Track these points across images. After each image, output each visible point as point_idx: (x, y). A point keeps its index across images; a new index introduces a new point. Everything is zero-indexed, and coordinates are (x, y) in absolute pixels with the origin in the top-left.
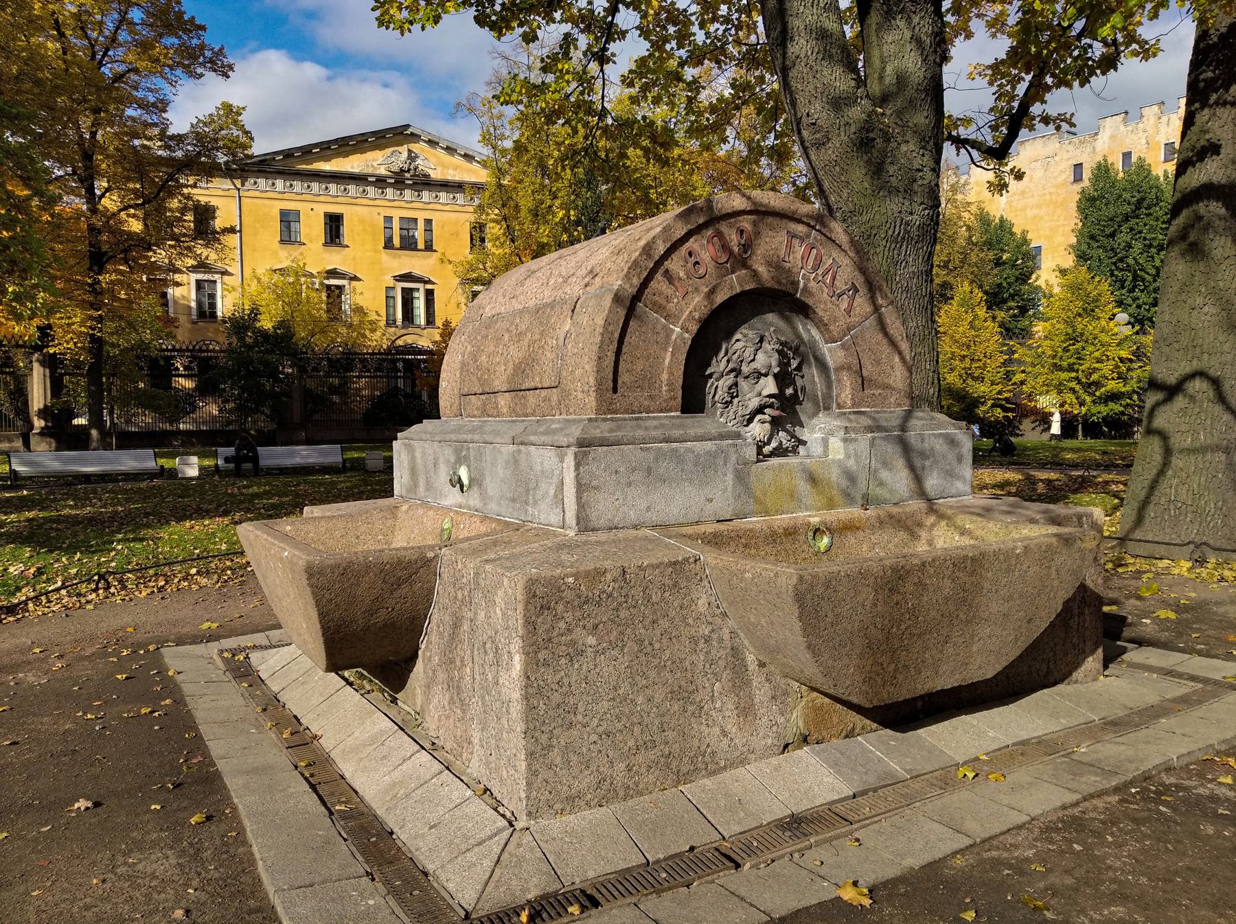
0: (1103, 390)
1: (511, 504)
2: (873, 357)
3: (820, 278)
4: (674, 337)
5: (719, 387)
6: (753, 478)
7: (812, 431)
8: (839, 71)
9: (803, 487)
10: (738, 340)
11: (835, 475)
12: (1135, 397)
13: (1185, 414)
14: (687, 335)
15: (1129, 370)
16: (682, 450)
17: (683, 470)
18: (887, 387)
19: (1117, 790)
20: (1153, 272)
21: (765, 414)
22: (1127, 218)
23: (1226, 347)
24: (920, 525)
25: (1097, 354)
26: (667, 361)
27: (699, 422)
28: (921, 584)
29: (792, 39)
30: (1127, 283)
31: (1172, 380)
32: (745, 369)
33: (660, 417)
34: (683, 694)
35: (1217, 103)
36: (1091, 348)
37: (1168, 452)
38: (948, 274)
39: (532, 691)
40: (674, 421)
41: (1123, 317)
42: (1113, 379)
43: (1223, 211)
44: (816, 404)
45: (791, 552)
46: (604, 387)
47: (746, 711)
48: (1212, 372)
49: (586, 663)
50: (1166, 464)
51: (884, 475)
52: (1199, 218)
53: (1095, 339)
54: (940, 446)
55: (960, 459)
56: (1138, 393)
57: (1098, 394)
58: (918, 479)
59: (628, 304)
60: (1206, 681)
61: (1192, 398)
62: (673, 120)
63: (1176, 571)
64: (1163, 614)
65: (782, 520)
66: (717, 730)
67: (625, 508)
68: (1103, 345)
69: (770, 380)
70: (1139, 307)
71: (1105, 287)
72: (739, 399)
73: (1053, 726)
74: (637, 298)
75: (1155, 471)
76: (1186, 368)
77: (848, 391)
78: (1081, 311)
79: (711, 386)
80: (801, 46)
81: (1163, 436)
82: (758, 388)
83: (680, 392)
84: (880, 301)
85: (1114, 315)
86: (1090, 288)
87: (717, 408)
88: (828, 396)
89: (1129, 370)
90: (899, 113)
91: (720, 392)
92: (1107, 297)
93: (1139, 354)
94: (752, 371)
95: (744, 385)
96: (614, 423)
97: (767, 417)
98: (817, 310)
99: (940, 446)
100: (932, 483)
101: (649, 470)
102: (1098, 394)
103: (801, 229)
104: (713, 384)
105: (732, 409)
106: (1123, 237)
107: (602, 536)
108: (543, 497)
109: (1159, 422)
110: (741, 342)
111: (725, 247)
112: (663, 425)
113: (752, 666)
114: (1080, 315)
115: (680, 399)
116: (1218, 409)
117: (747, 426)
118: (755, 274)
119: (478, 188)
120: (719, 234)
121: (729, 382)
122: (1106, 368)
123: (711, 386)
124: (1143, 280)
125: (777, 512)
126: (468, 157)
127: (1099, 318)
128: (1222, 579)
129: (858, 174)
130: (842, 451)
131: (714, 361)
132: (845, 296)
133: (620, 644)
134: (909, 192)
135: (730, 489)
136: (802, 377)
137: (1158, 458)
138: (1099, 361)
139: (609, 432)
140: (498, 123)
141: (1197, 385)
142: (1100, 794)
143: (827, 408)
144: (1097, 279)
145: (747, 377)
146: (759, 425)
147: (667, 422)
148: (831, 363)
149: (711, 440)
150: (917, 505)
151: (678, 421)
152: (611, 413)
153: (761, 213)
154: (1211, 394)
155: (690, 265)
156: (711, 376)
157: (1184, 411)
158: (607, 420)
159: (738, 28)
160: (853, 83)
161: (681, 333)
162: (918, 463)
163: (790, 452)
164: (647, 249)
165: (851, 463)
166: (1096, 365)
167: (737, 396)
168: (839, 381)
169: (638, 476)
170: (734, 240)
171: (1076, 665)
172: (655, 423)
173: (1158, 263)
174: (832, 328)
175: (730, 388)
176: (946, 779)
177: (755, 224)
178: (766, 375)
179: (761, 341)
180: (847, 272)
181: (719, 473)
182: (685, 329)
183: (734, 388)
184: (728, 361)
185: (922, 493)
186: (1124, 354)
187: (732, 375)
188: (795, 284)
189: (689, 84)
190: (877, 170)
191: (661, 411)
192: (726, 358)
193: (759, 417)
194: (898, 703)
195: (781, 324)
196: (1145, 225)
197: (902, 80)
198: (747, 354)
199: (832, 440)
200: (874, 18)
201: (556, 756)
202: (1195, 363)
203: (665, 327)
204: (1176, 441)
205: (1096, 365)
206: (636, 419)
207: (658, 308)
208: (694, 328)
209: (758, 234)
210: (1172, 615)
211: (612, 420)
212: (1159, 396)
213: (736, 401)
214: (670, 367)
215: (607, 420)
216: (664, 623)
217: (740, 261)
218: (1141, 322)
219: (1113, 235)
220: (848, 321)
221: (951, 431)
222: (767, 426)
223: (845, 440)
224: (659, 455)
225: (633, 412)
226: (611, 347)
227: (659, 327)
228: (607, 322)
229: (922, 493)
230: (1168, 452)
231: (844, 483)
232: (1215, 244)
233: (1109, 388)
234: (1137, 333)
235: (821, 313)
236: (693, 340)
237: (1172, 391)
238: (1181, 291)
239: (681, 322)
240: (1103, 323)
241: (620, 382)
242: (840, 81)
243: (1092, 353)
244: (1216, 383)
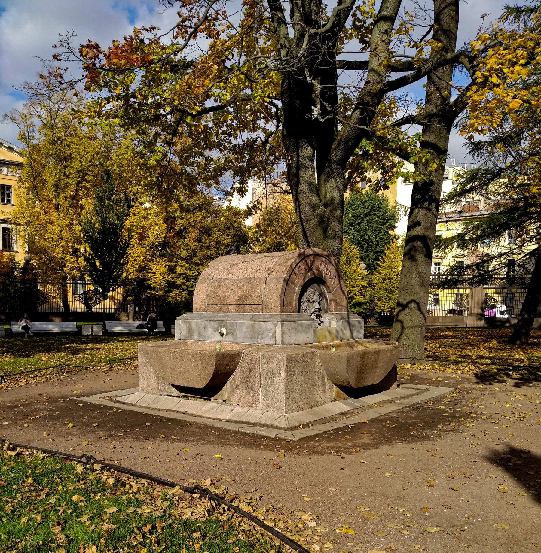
0: (354, 301)
1: (250, 339)
5: (304, 306)
7: (325, 318)
8: (315, 196)
9: (327, 334)
11: (334, 331)
12: (368, 305)
13: (409, 315)
15: (366, 291)
18: (342, 306)
19: (408, 407)
20: (376, 243)
22: (366, 216)
23: (422, 292)
24: (354, 346)
25: (352, 283)
28: (368, 357)
29: (301, 184)
30: (365, 248)
31: (405, 303)
32: (311, 300)
34: (313, 386)
35: (420, 207)
36: (350, 280)
37: (403, 328)
38: (281, 238)
39: (287, 382)
41: (363, 265)
42: (359, 296)
43: (422, 245)
47: (324, 391)
48: (417, 301)
49: (296, 376)
50: (402, 332)
51: (345, 331)
52: (414, 247)
53: (351, 276)
54: (356, 323)
55: (361, 327)
56: (369, 303)
57: (352, 303)
58: (352, 333)
60: (422, 389)
61: (411, 309)
62: (138, 140)
63: (406, 367)
64: (406, 377)
65: (324, 343)
66: (319, 396)
68: (355, 279)
69: (317, 303)
70: (369, 260)
71: (356, 251)
73: (391, 397)
74: (288, 280)
75: (399, 334)
76: (409, 299)
77: (333, 307)
78: (345, 262)
80: (303, 187)
81: (401, 322)
82: (314, 306)
84: (341, 280)
85: (360, 264)
86: (350, 250)
88: (327, 308)
89: (366, 291)
90: (331, 211)
92: (358, 255)
93: (370, 285)
95: (310, 305)
99: (356, 323)
100: (355, 334)
101: (296, 329)
102: (352, 303)
103: (324, 259)
105: (307, 312)
106: (364, 226)
107: (286, 346)
108: (267, 336)
109: (400, 317)
110: (309, 291)
111: (307, 265)
113: (326, 380)
114: (344, 264)
116: (419, 313)
118: (314, 273)
119: (19, 165)
120: (306, 261)
122: (356, 290)
124: (372, 247)
126: (10, 149)
127: (353, 266)
128: (421, 369)
129: (319, 233)
133: (302, 372)
134: (334, 238)
137: (400, 330)
138: (353, 287)
140: (31, 129)
141: (413, 305)
142: (405, 407)
143: (327, 312)
144: (353, 247)
150: (352, 341)
153: (316, 255)
154: (417, 308)
157: (408, 314)
159: (230, 136)
160: (319, 201)
161: (297, 290)
162: (352, 328)
164: (291, 266)
165: (338, 328)
166: (352, 289)
168: (330, 304)
169: (294, 330)
170: (309, 262)
171: (391, 385)
173: (378, 239)
176: (370, 407)
177: (314, 258)
180: (334, 272)
182: (299, 289)
183: (307, 307)
185: (352, 338)
186: (364, 284)
189: (206, 158)
190: (325, 231)
194: (360, 388)
195: (318, 287)
196: (373, 219)
197: (332, 199)
199: (332, 321)
200: (323, 177)
201: (290, 398)
202: (412, 297)
204: (406, 324)
205: (352, 289)
207: (293, 283)
208: (301, 288)
209: (314, 261)
210: (409, 378)
212: (401, 308)
216: (310, 367)
217: (310, 269)
218: (371, 268)
219: (359, 224)
221: (359, 319)
223: (337, 322)
224: (298, 325)
228: (283, 287)
229: (352, 338)
230: (403, 328)
231: (336, 333)
232: (419, 256)
233: (357, 300)
234: (369, 274)
237: (404, 307)
238: (408, 272)
240: (355, 268)
242: (314, 199)
243: (350, 283)
244: (418, 304)
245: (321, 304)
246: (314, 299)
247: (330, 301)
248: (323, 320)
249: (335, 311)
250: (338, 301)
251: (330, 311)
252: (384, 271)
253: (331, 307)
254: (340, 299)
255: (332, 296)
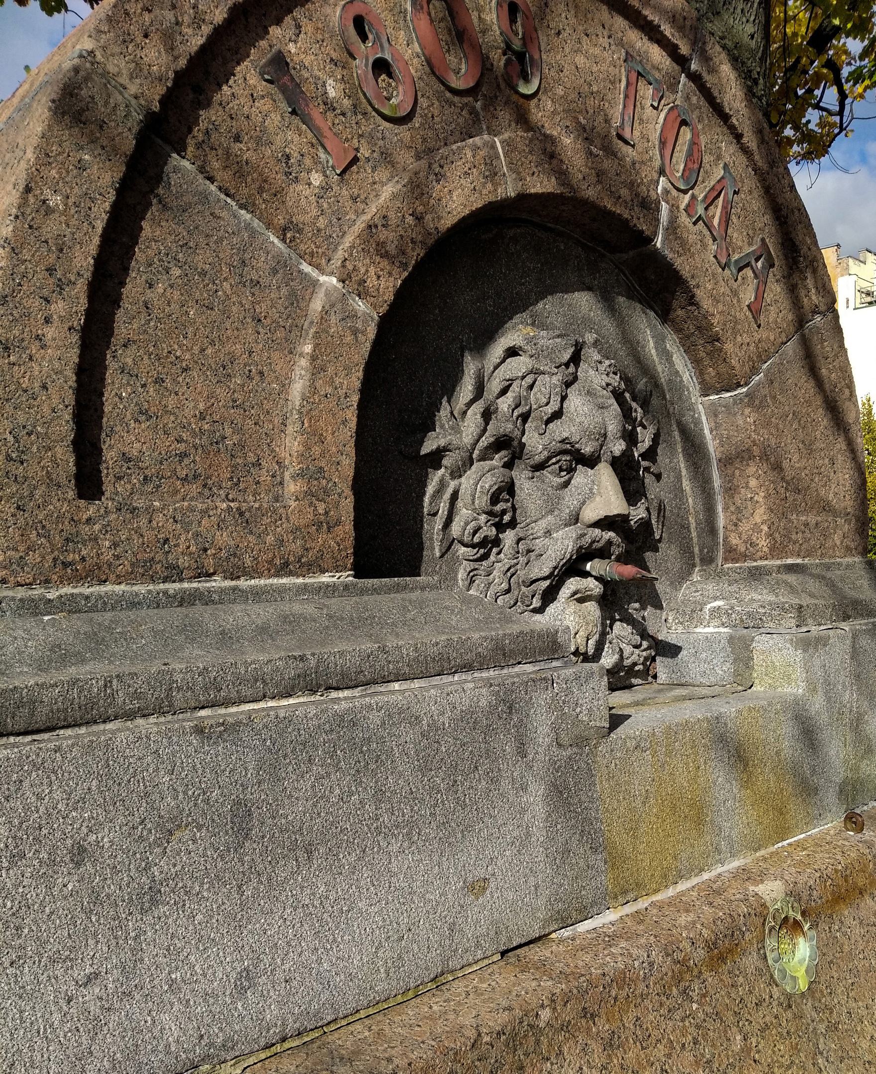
2: (801, 435)
3: (700, 210)
4: (317, 305)
6: (602, 786)
7: (693, 614)
10: (512, 352)
14: (361, 306)
16: (375, 718)
17: (379, 796)
18: (826, 508)
19: (360, 85)
21: (586, 574)
26: (297, 388)
27: (421, 605)
33: (282, 591)
40: (334, 603)
44: (686, 551)
45: (730, 1018)
46: (34, 470)
59: (129, 143)
67: (136, 1007)
69: (605, 475)
72: (518, 531)
77: (760, 515)
79: (439, 492)
82: (570, 500)
83: (348, 504)
87: (456, 560)
91: (464, 513)
94: (555, 446)
96: (79, 623)
97: (591, 583)
98: (699, 293)
104: (442, 486)
105: (500, 561)
112: (290, 621)
115: (347, 528)
117: (540, 610)
121: (489, 482)
123: (439, 492)
125: (666, 880)
130: (799, 673)
131: (444, 413)
132: (748, 272)
135: (539, 834)
136: (658, 477)
139: (42, 666)
143: (708, 560)
145: (539, 467)
146: (573, 606)
147: (310, 609)
148: (712, 445)
149: (468, 667)
151: (346, 605)
152: (79, 578)
155: (361, 67)
156: (436, 458)
158: (50, 606)
163: (637, 674)
165: (817, 704)
167: (513, 524)
168: (730, 490)
172: (261, 613)
174: (729, 347)
175: (495, 499)
178: (591, 462)
179: (576, 359)
181: (505, 785)
184: (487, 415)
187: (498, 459)
188: (649, 207)
191: (284, 569)
192: (478, 407)
193: (573, 584)
195: (609, 326)
198: (537, 396)
199: (761, 643)
203: (280, 266)
206: (185, 600)
211: (70, 606)
213: (509, 537)
214: (308, 411)
215: (50, 606)
220: (757, 336)
222: (592, 608)
223: (808, 644)
225: (174, 573)
226: (59, 307)
227: (262, 263)
235: (706, 304)
236: (385, 323)
239: (340, 254)
241: (110, 455)
245: (654, 489)
246: (560, 430)
247: (726, 462)
248: (670, 634)
249: (776, 550)
250: (794, 462)
251: (732, 554)
252: (831, 495)
253: (738, 515)
254: (809, 449)
255: (747, 418)
